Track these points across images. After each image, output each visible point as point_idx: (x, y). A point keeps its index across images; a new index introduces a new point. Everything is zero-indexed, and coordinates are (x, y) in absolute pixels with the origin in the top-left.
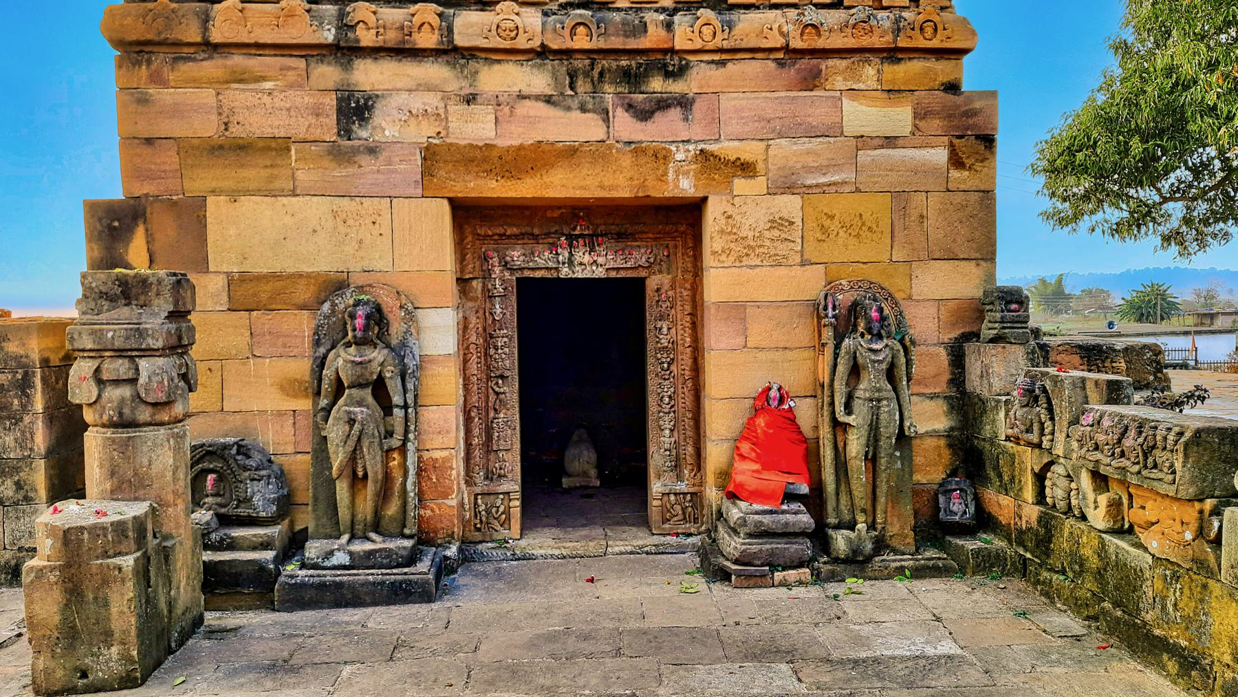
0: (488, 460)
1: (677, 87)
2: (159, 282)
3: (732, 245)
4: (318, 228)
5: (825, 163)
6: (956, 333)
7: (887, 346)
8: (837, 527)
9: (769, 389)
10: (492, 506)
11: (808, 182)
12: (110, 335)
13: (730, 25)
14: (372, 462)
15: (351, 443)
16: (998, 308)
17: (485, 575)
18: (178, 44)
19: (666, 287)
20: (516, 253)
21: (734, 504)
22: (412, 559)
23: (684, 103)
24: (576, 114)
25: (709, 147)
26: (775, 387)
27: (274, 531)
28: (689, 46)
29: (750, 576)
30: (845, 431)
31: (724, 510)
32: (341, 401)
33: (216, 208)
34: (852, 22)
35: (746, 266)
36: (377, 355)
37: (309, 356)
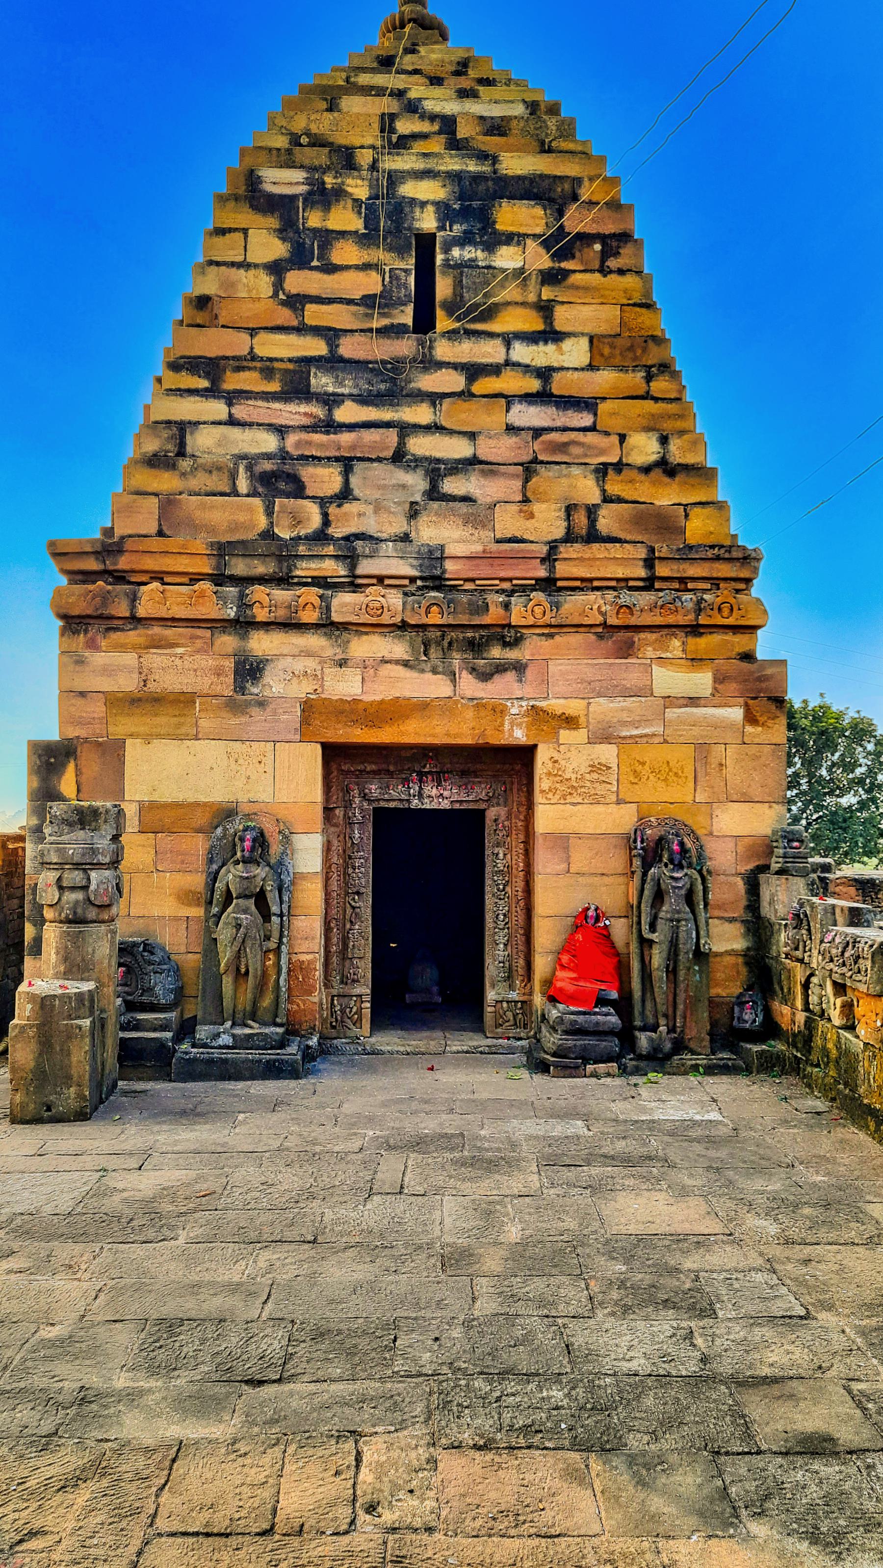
0: (344, 966)
1: (512, 654)
2: (107, 811)
3: (558, 785)
4: (214, 766)
5: (637, 718)
6: (751, 866)
7: (686, 874)
8: (644, 1029)
9: (588, 909)
10: (346, 1007)
11: (623, 734)
12: (71, 852)
13: (557, 606)
14: (253, 961)
15: (237, 945)
16: (781, 845)
17: (340, 1063)
18: (111, 618)
19: (503, 818)
20: (373, 787)
21: (555, 1006)
22: (282, 1044)
23: (519, 668)
24: (429, 676)
25: (537, 703)
26: (593, 907)
27: (173, 1015)
28: (523, 622)
29: (565, 1067)
30: (651, 947)
31: (546, 1012)
32: (230, 909)
33: (133, 750)
34: (660, 603)
35: (570, 803)
36: (260, 872)
37: (202, 872)
